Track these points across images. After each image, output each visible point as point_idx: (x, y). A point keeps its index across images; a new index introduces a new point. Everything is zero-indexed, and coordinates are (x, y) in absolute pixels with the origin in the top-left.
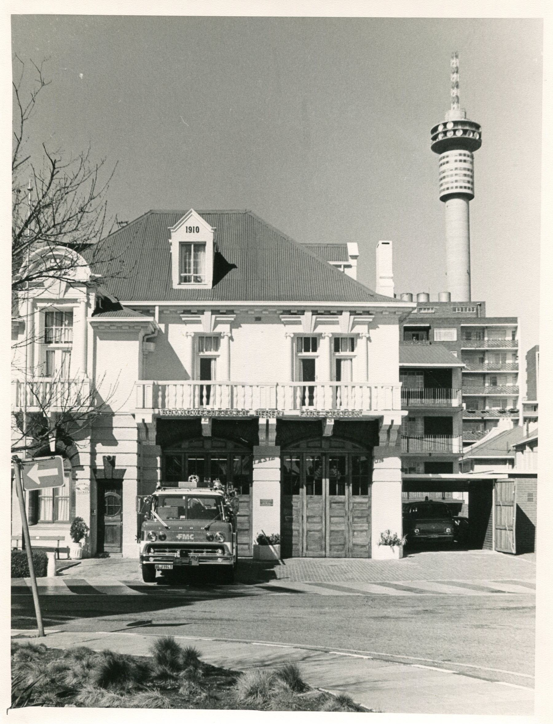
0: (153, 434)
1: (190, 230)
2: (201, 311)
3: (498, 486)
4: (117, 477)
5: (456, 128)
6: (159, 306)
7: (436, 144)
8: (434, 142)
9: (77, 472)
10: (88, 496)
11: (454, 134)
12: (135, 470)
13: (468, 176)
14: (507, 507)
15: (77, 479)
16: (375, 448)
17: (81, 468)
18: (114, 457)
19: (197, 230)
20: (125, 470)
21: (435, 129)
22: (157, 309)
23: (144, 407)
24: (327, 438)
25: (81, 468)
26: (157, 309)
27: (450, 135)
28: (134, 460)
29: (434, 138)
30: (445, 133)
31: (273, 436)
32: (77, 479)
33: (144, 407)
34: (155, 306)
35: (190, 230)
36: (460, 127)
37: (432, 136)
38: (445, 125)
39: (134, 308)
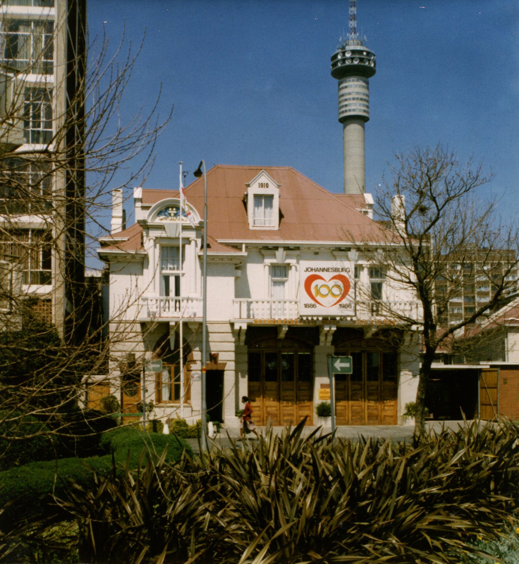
0: (243, 338)
1: (262, 185)
2: (276, 248)
3: (483, 374)
4: (220, 368)
5: (354, 56)
6: (246, 244)
7: (335, 70)
8: (335, 68)
9: (192, 365)
10: (200, 383)
11: (352, 62)
12: (233, 364)
13: (365, 100)
14: (491, 390)
15: (191, 371)
16: (316, 347)
17: (194, 362)
18: (218, 354)
19: (267, 185)
20: (226, 364)
21: (335, 56)
22: (244, 246)
23: (240, 318)
24: (280, 340)
25: (194, 362)
26: (244, 246)
27: (348, 63)
28: (232, 356)
29: (334, 65)
30: (344, 60)
31: (330, 338)
32: (191, 371)
33: (240, 318)
34: (242, 244)
35: (262, 185)
36: (357, 56)
37: (332, 63)
38: (344, 53)
39: (227, 245)
